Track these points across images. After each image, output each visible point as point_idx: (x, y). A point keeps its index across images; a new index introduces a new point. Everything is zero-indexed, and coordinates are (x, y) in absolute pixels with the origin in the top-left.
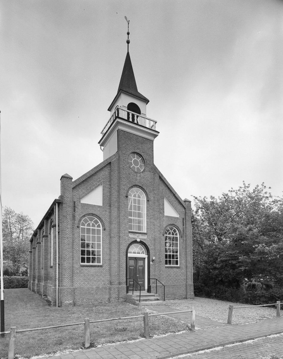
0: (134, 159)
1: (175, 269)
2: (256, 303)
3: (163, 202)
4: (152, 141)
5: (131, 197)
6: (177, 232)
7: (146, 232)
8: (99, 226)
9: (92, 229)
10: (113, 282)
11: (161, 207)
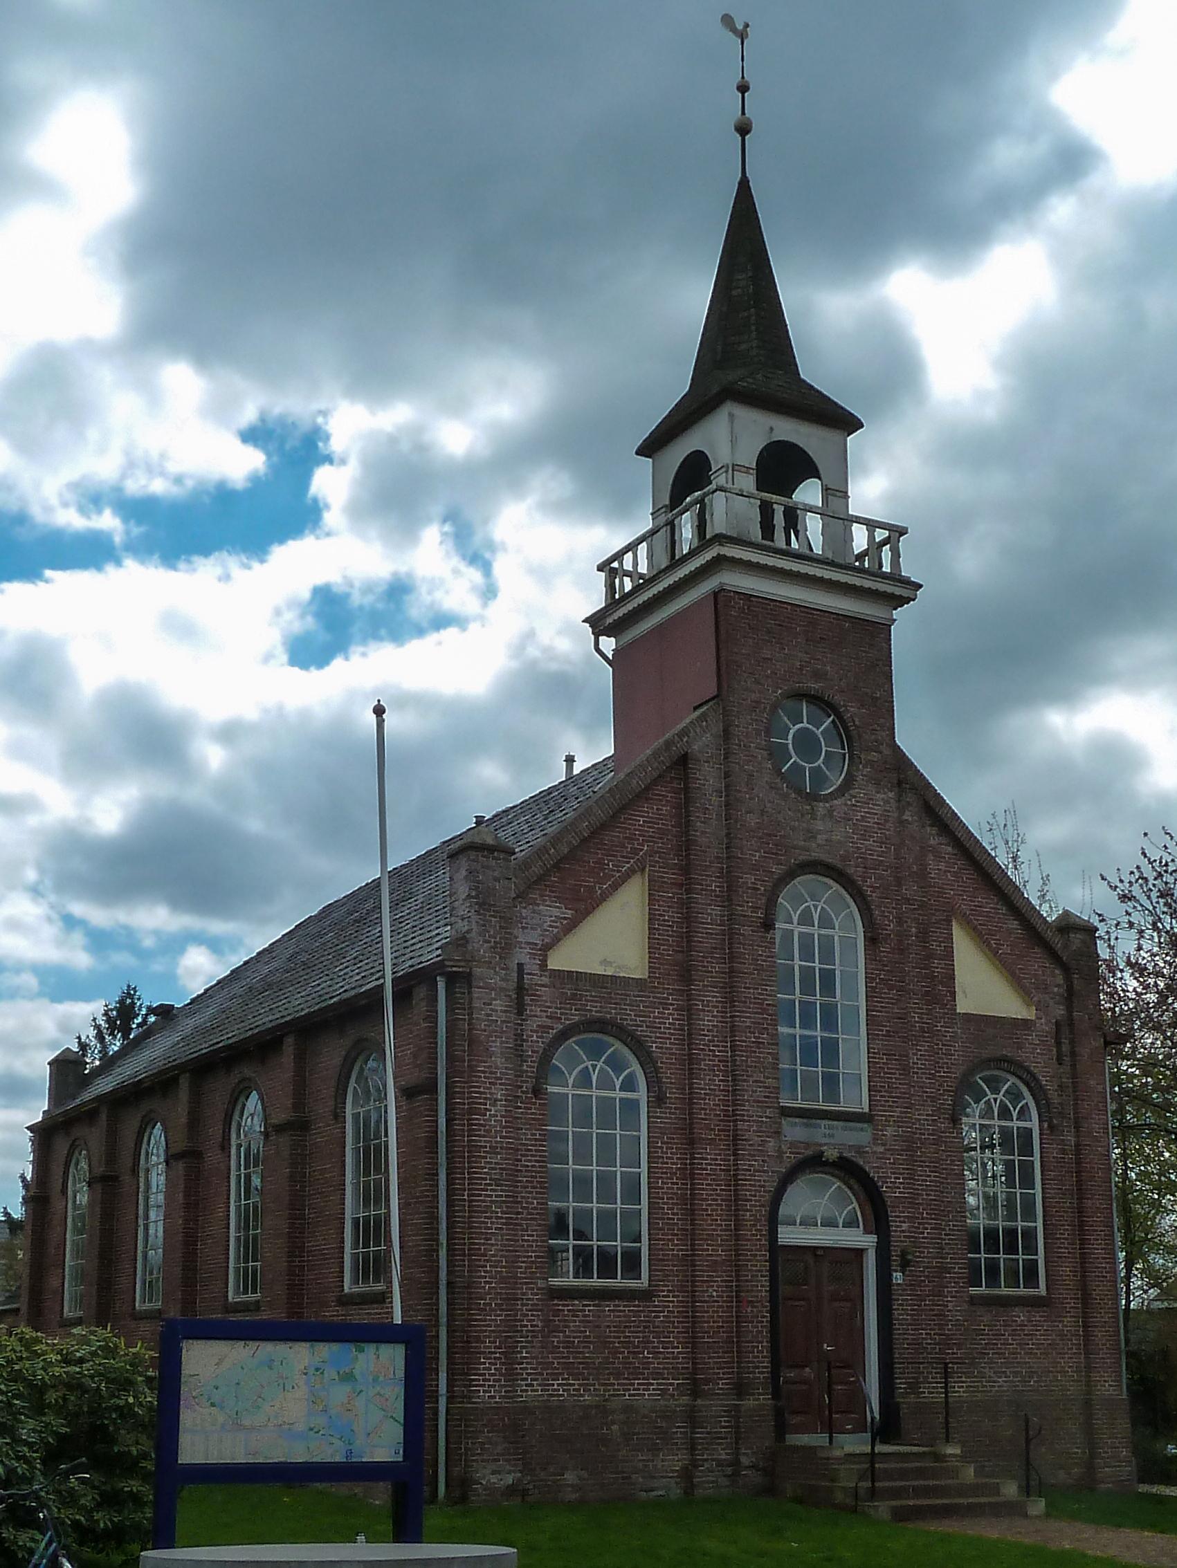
0: (816, 764)
1: (1020, 1315)
2: (868, 961)
3: (950, 938)
4: (882, 630)
5: (789, 924)
6: (1029, 1100)
7: (867, 1110)
8: (629, 1085)
9: (621, 1099)
10: (707, 1381)
11: (938, 966)
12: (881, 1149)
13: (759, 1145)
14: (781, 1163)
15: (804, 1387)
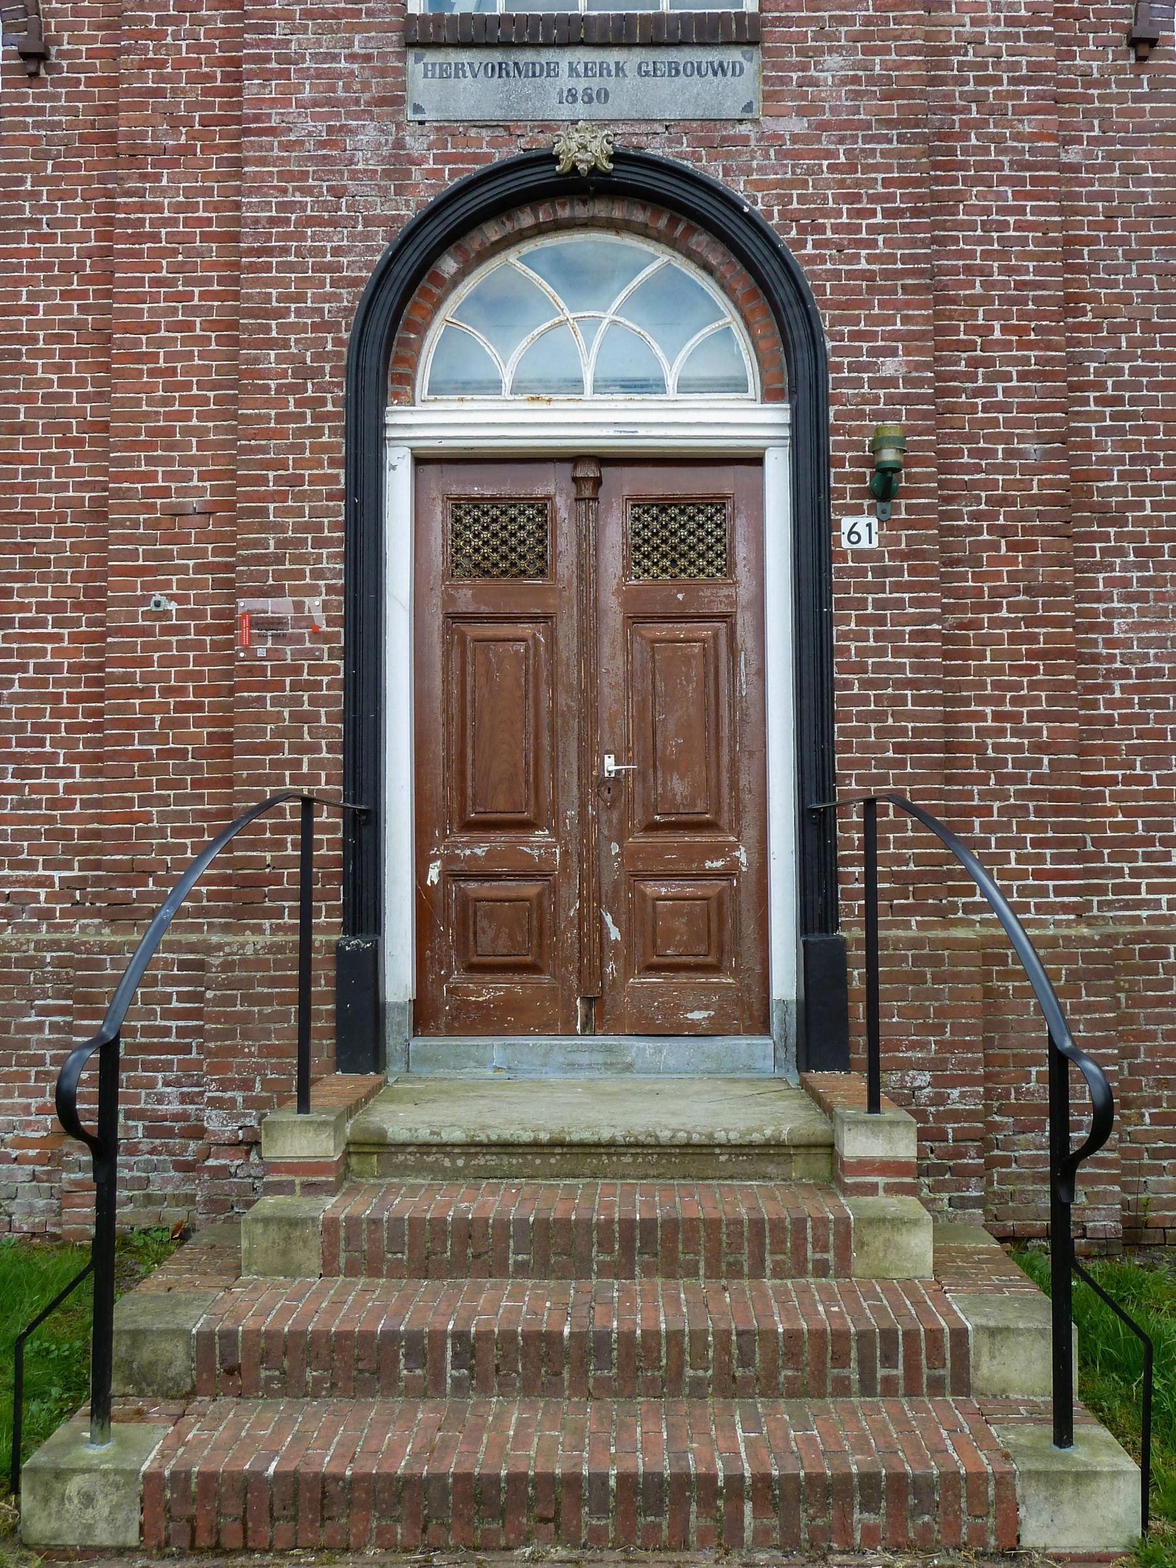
12: (799, 125)
13: (322, 144)
14: (399, 190)
15: (530, 889)
